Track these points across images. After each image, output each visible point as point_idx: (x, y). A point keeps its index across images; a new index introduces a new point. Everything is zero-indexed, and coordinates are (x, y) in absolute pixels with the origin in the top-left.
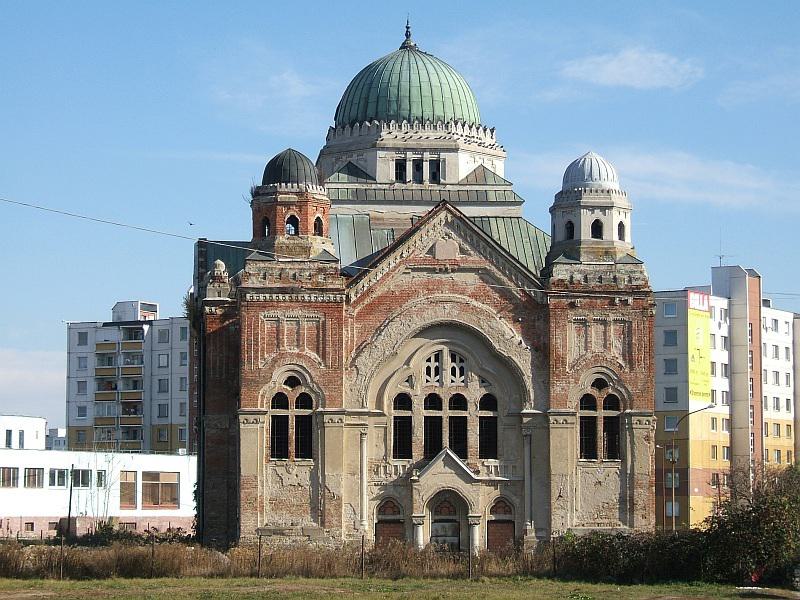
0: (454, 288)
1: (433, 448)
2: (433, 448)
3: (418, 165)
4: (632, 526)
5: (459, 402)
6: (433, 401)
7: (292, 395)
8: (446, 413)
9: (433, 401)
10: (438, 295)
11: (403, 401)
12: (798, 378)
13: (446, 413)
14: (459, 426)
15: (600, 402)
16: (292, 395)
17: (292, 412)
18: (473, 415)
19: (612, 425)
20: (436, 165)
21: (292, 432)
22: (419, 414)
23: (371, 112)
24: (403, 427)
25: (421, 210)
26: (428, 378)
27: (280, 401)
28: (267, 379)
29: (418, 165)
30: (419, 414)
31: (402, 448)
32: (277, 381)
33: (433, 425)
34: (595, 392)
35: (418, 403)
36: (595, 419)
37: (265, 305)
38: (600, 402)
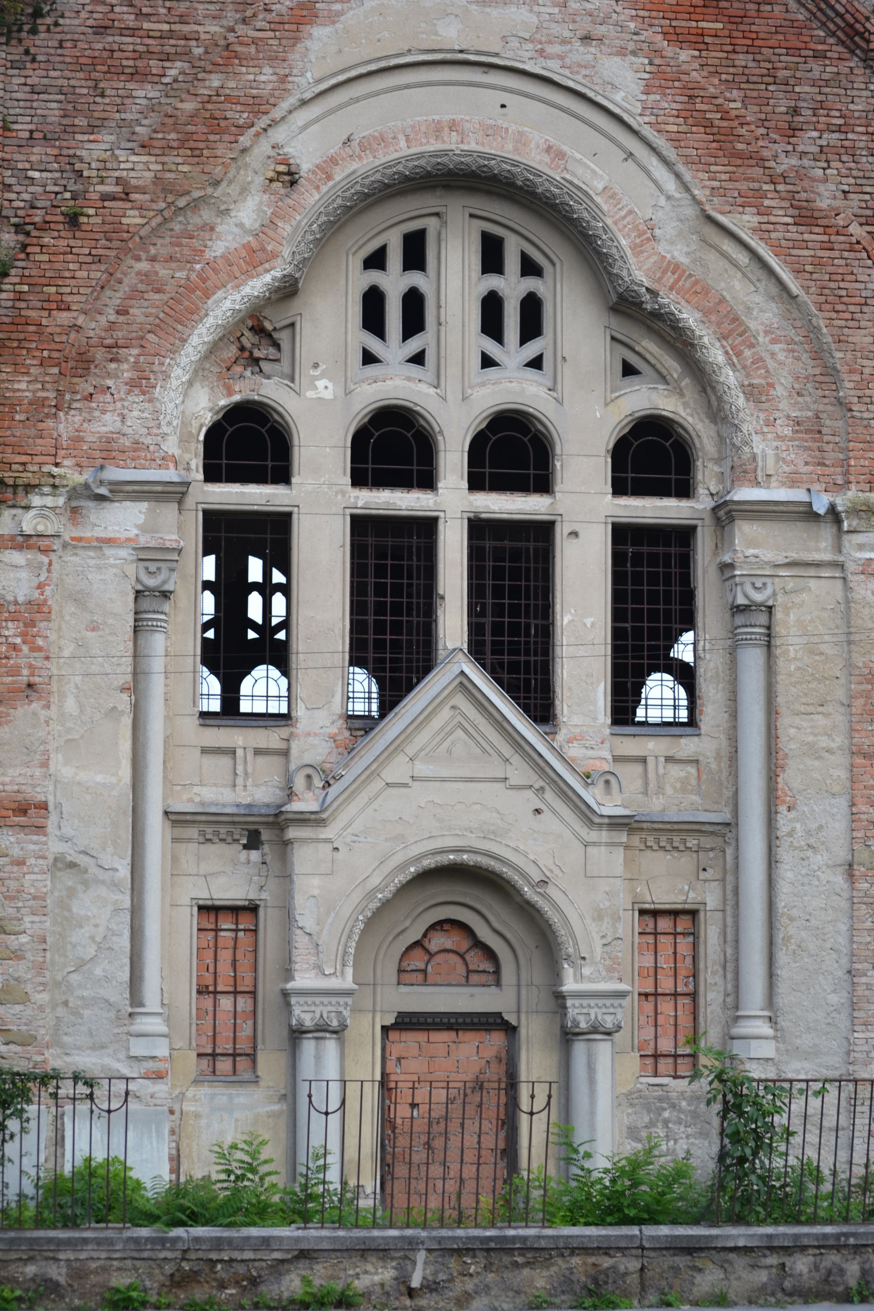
5: (513, 451)
6: (391, 446)
9: (391, 446)
11: (249, 442)
14: (516, 565)
18: (584, 513)
22: (322, 500)
26: (491, 347)
30: (322, 500)
33: (390, 559)
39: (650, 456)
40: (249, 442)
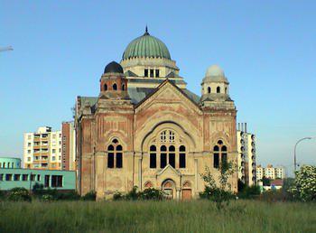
0: (171, 109)
1: (163, 165)
2: (163, 165)
3: (152, 72)
4: (211, 205)
5: (172, 148)
6: (163, 148)
7: (115, 145)
8: (168, 152)
10: (165, 112)
11: (153, 148)
12: (275, 140)
13: (115, 152)
14: (172, 157)
15: (220, 149)
16: (115, 145)
17: (115, 152)
18: (177, 152)
19: (119, 156)
20: (158, 71)
21: (220, 157)
22: (158, 153)
23: (136, 54)
24: (153, 157)
25: (156, 86)
27: (111, 148)
28: (107, 141)
29: (152, 72)
30: (158, 153)
31: (153, 165)
32: (110, 142)
33: (163, 156)
34: (218, 145)
35: (158, 148)
36: (113, 154)
37: (106, 114)
38: (220, 149)
39: (182, 148)
40: (153, 148)
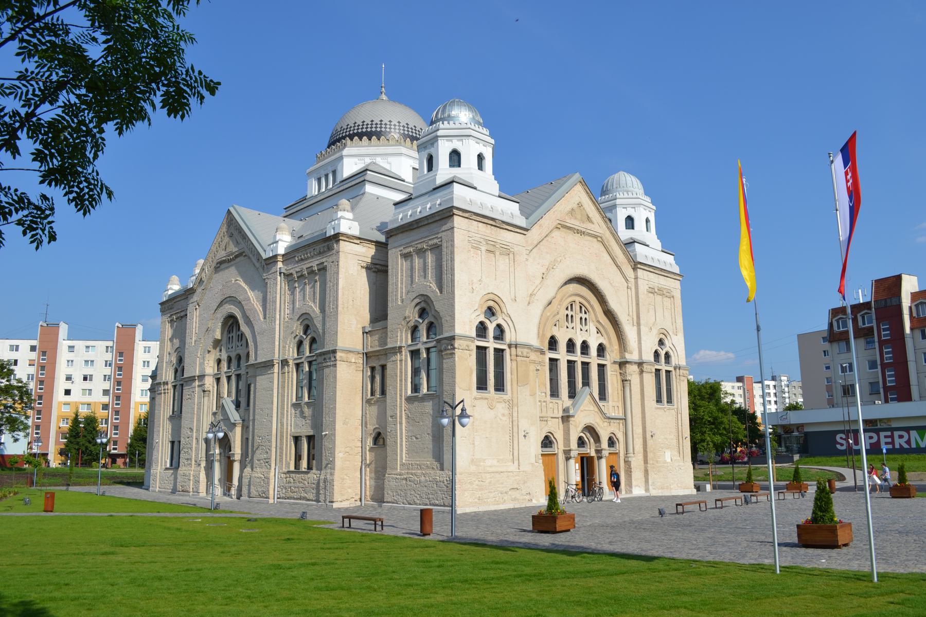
14: (585, 365)
